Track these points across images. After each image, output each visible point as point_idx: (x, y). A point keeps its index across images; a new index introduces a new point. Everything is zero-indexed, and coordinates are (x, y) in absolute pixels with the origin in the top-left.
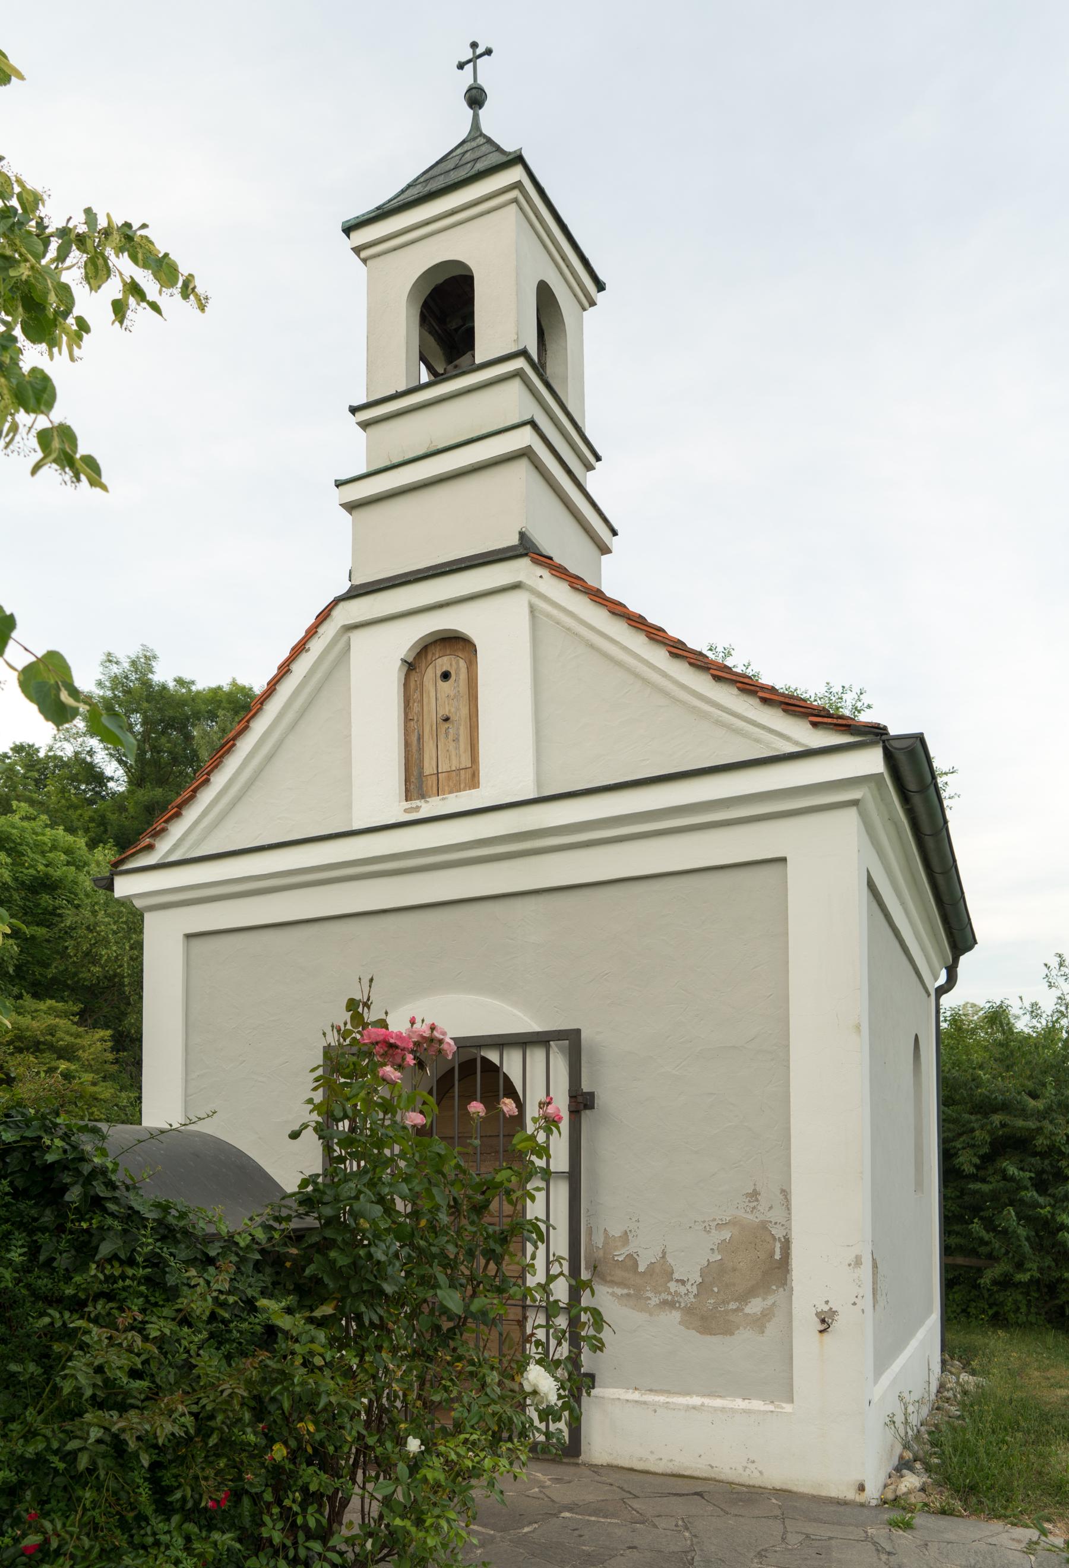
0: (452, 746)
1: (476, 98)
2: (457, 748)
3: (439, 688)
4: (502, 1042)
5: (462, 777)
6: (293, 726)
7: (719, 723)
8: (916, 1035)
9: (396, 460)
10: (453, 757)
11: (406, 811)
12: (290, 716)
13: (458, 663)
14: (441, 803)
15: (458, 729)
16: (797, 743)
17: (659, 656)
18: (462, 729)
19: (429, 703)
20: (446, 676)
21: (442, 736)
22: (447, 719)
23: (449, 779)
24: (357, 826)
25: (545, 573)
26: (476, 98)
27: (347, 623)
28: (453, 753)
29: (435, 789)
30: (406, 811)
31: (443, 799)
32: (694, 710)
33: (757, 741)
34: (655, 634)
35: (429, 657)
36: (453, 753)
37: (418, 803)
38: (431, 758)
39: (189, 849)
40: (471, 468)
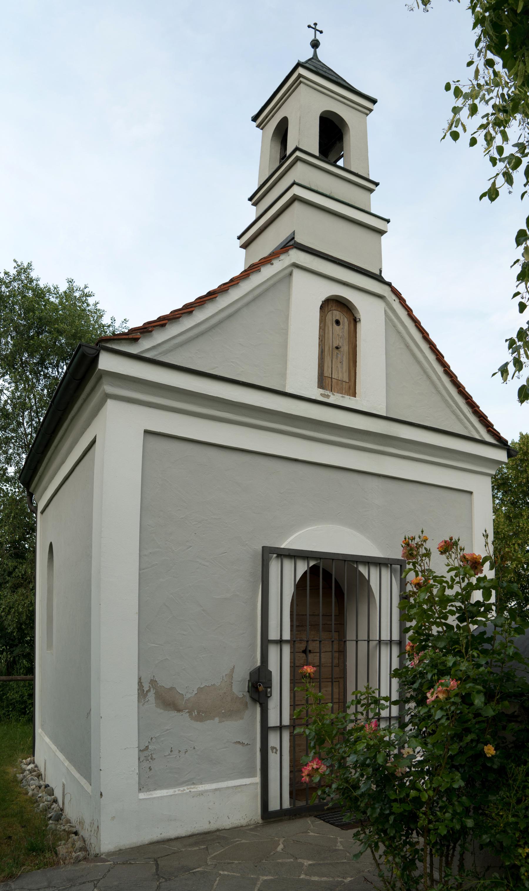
0: (339, 365)
1: (315, 44)
2: (342, 368)
3: (334, 327)
4: (369, 562)
5: (344, 387)
6: (248, 304)
7: (454, 412)
8: (96, 436)
9: (313, 187)
10: (340, 372)
11: (321, 394)
12: (250, 297)
13: (344, 318)
14: (341, 399)
15: (342, 357)
16: (481, 436)
17: (439, 370)
18: (344, 357)
19: (328, 333)
20: (338, 322)
21: (335, 357)
22: (337, 348)
23: (337, 384)
24: (289, 390)
25: (397, 301)
26: (315, 44)
27: (297, 262)
28: (340, 369)
29: (330, 388)
30: (321, 394)
31: (343, 397)
32: (446, 401)
33: (466, 428)
34: (439, 357)
35: (330, 307)
36: (340, 369)
37: (327, 393)
38: (328, 367)
39: (160, 354)
40: (342, 216)
